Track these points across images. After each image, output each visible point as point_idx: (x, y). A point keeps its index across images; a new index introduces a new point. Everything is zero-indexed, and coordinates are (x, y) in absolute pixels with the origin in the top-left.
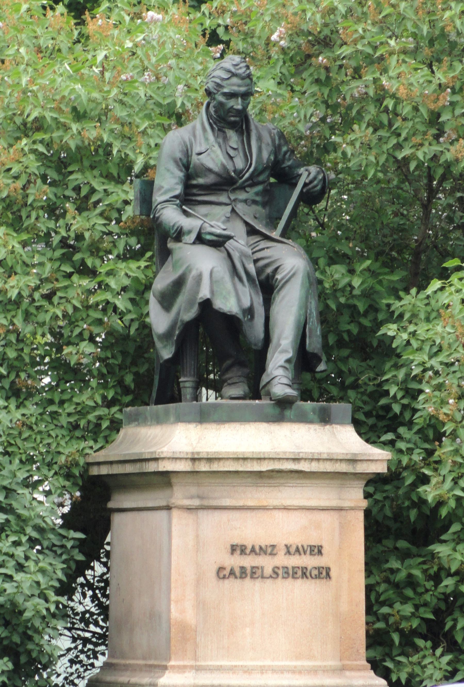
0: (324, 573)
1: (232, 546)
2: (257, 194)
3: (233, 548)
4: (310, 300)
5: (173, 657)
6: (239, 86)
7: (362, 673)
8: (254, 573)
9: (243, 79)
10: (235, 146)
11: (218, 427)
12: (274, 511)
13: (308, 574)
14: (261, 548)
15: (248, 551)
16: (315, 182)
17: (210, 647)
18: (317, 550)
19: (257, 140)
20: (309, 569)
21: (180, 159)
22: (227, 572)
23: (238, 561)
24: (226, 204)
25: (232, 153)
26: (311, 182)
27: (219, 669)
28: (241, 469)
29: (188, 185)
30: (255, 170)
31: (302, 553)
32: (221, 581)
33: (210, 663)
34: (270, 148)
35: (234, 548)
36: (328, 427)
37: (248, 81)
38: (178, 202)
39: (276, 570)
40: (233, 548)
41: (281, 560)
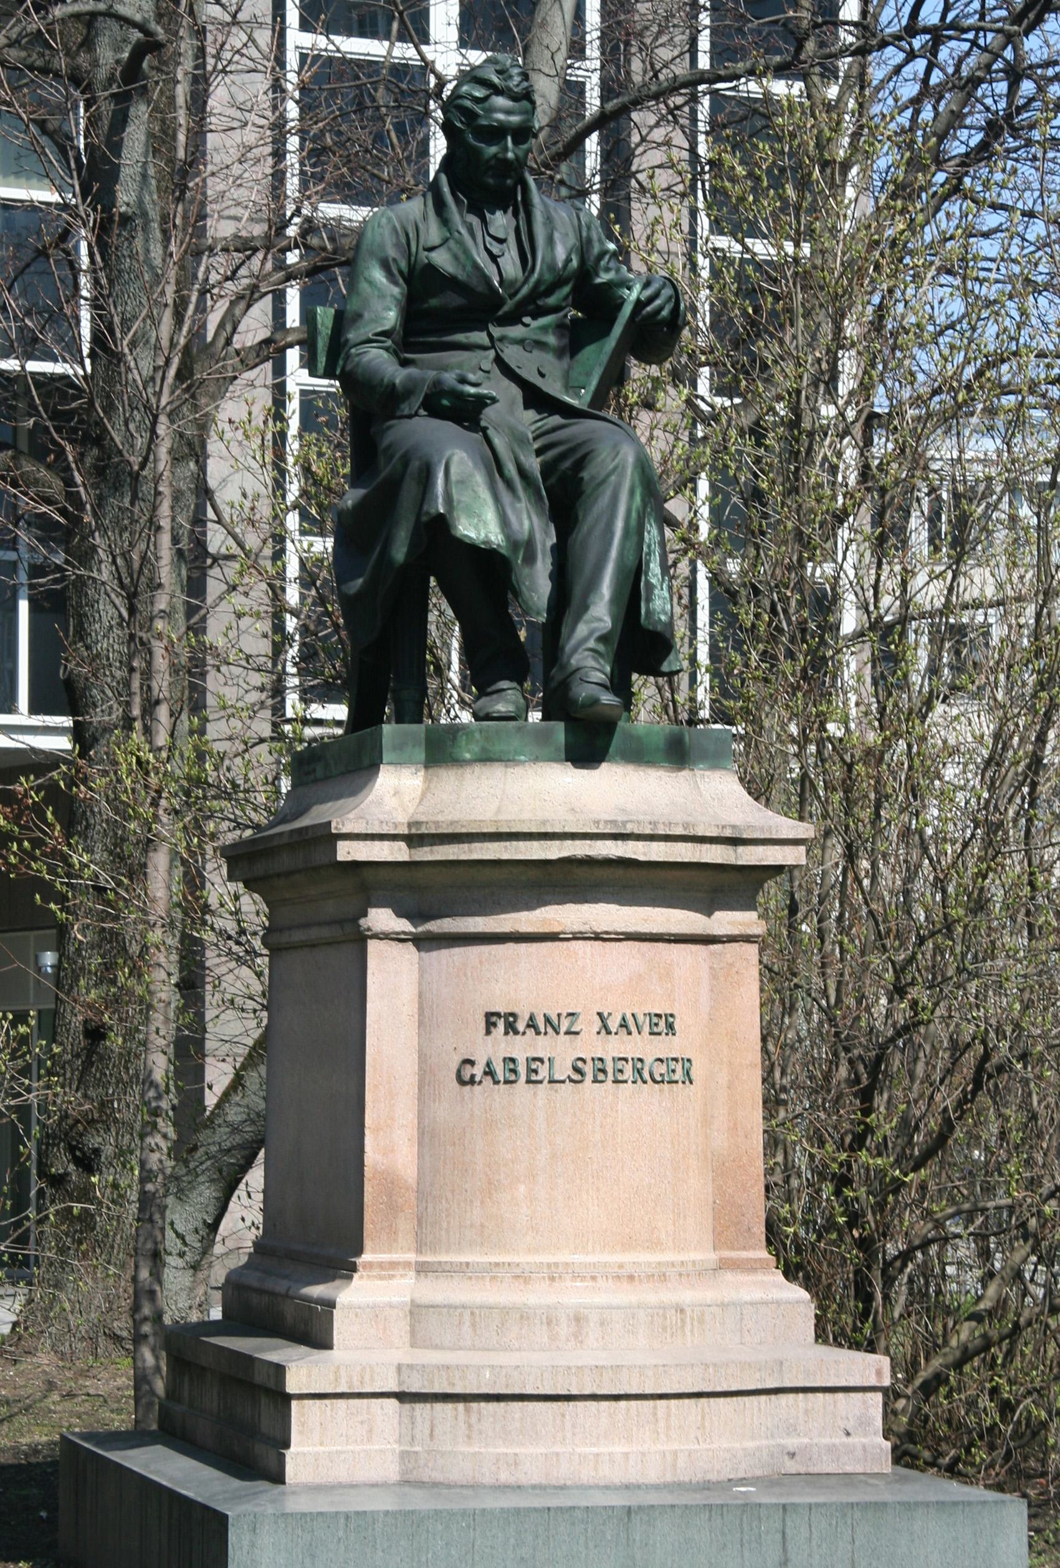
0: (676, 1073)
1: (489, 1015)
2: (544, 329)
3: (490, 1020)
4: (647, 526)
5: (368, 1243)
6: (508, 112)
7: (760, 1277)
8: (533, 1072)
9: (515, 98)
10: (501, 235)
11: (460, 771)
12: (574, 942)
13: (646, 1076)
14: (548, 1020)
15: (521, 1026)
16: (658, 302)
17: (445, 1225)
18: (664, 1024)
19: (545, 224)
20: (649, 1060)
21: (394, 260)
22: (478, 1071)
23: (498, 1047)
24: (484, 348)
25: (495, 249)
26: (651, 299)
27: (464, 1269)
28: (505, 857)
29: (411, 310)
30: (538, 283)
31: (633, 1029)
32: (468, 1087)
33: (443, 1258)
34: (572, 240)
35: (494, 1019)
36: (685, 773)
37: (525, 104)
38: (389, 343)
39: (580, 1064)
40: (490, 1020)
41: (591, 1045)
